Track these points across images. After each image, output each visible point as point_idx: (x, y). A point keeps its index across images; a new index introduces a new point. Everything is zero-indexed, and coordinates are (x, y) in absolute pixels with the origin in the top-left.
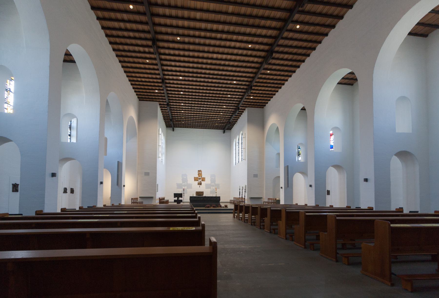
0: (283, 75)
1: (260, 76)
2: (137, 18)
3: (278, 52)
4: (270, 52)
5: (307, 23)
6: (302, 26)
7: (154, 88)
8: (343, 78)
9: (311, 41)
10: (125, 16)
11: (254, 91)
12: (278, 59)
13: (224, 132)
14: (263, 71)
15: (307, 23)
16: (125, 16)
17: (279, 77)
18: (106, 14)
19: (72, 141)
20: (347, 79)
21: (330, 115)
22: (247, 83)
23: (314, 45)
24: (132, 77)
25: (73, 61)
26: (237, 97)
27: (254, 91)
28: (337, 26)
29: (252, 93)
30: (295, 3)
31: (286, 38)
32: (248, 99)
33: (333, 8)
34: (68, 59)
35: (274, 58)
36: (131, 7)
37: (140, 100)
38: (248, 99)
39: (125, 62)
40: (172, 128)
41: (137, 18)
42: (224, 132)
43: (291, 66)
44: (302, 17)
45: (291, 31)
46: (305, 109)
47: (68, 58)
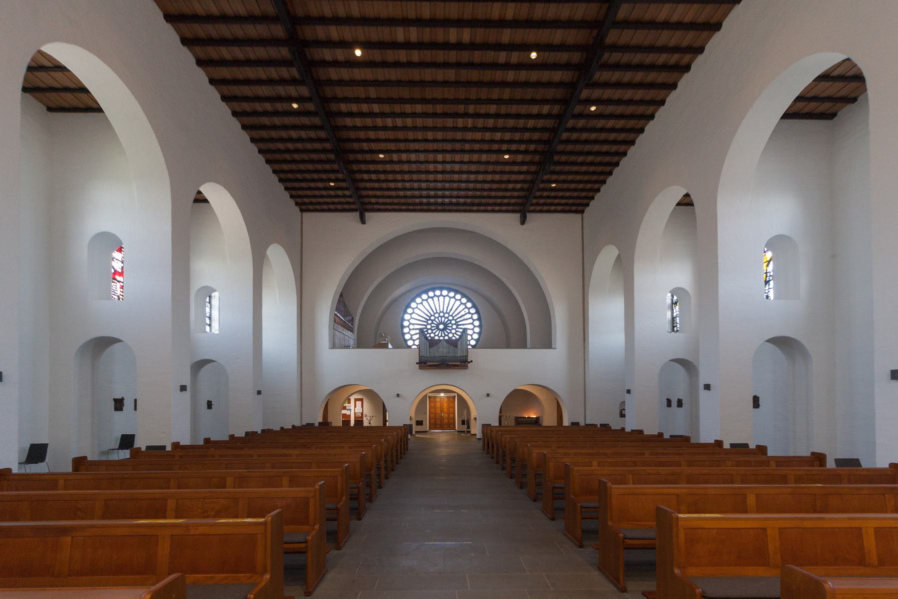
0: (594, 173)
1: (565, 136)
2: (305, 120)
3: (562, 153)
4: (583, 69)
5: (609, 102)
6: (601, 107)
7: (324, 176)
8: (799, 99)
9: (632, 116)
10: (287, 120)
11: (558, 168)
12: (617, 66)
13: (523, 221)
14: (542, 186)
15: (609, 102)
16: (287, 120)
17: (620, 123)
18: (264, 134)
19: (213, 331)
20: (814, 99)
21: (663, 279)
22: (540, 147)
23: (631, 136)
24: (223, 63)
25: (206, 201)
26: (513, 201)
27: (558, 168)
28: (694, 66)
29: (553, 173)
30: (606, 6)
31: (574, 129)
32: (544, 190)
33: (679, 34)
34: (201, 199)
35: (606, 66)
36: (295, 106)
37: (302, 211)
38: (544, 190)
39: (283, 171)
40: (357, 214)
41: (305, 120)
42: (523, 221)
43: (623, 130)
44: (597, 93)
45: (580, 116)
46: (691, 204)
47: (199, 197)
